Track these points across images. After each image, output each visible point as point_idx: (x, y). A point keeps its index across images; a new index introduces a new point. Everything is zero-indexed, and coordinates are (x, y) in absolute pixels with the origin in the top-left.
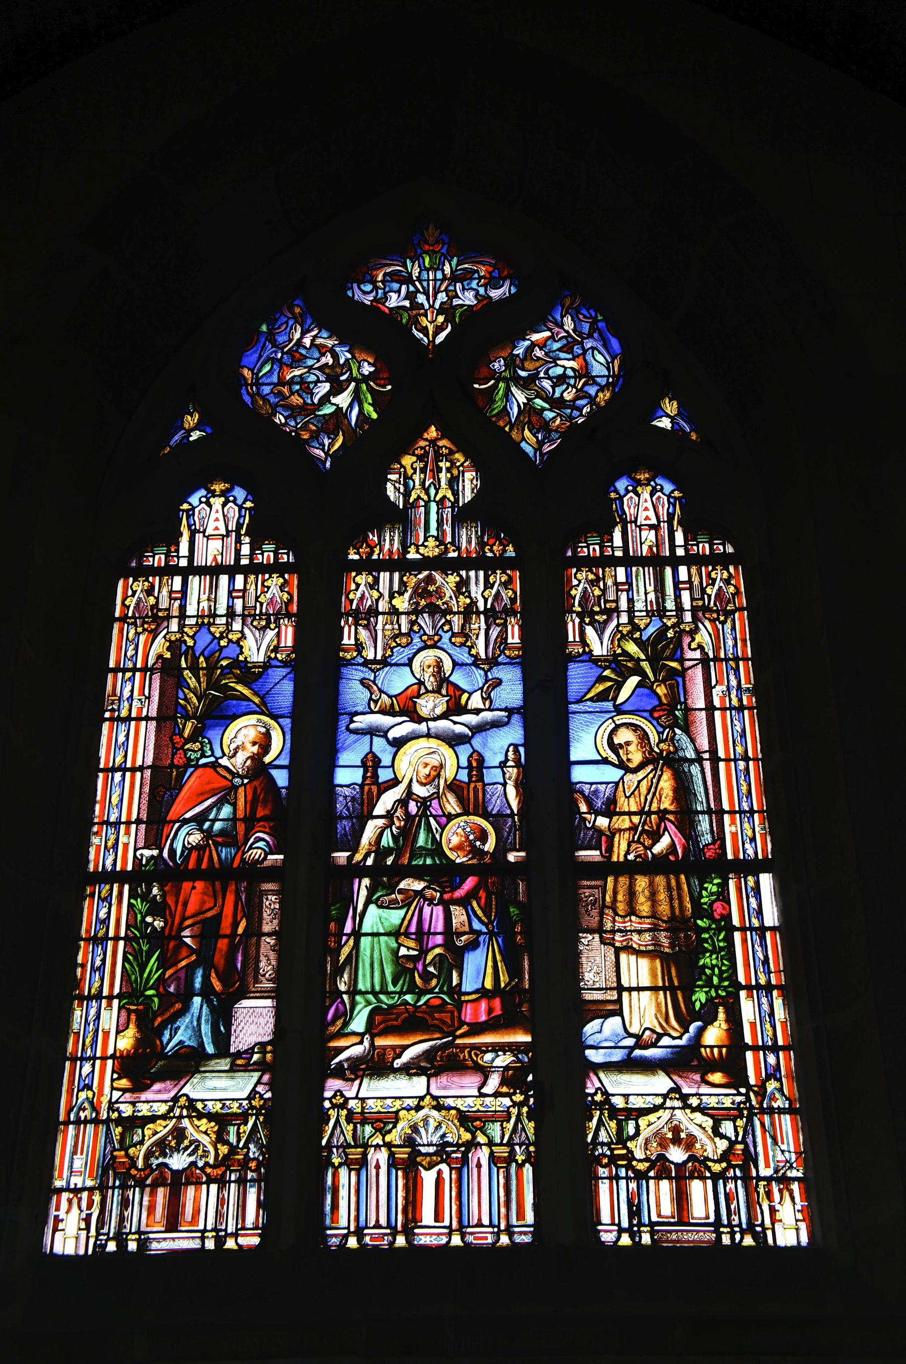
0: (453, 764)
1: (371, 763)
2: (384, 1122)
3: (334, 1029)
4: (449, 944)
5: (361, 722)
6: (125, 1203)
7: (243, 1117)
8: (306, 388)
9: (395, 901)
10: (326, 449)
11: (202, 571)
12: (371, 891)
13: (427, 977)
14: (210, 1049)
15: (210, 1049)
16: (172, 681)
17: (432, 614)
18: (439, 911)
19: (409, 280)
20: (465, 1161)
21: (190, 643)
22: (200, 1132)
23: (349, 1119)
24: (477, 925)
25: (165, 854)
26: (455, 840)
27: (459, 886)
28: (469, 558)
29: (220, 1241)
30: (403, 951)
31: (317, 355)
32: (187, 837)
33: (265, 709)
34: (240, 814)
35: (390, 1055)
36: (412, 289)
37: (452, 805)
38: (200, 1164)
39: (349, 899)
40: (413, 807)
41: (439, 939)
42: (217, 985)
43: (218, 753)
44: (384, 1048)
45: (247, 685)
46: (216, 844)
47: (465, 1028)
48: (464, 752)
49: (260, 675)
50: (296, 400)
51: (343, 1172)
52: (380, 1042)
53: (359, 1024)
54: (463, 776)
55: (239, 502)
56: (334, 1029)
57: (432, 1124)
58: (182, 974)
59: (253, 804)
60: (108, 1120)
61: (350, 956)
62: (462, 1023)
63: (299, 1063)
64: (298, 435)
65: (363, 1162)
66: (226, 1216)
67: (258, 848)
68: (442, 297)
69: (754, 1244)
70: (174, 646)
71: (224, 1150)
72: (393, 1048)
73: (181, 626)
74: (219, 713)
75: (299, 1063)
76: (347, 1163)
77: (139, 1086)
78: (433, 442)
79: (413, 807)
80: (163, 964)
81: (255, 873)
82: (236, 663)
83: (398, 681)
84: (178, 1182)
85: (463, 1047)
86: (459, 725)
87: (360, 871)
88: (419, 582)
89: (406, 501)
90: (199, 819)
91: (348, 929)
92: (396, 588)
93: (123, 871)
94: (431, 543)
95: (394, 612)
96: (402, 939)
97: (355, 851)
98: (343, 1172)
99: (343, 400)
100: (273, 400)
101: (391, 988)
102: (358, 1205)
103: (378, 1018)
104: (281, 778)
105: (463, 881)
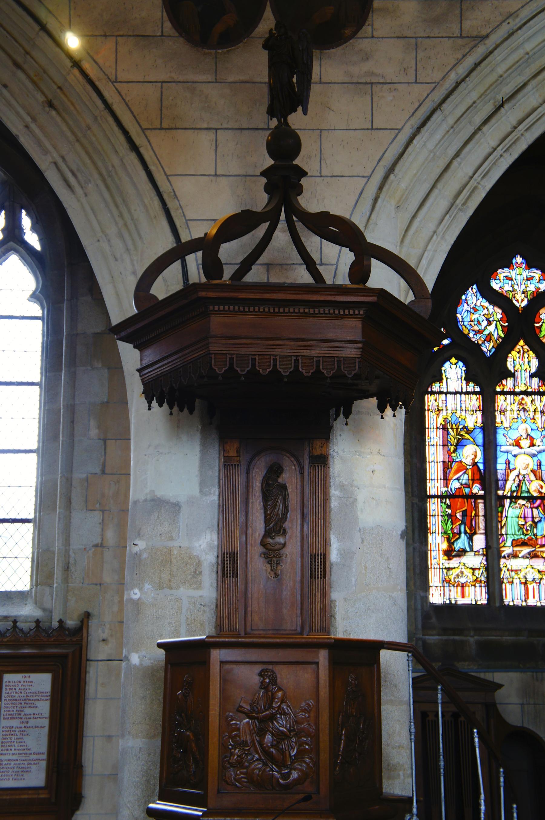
0: (532, 464)
1: (508, 463)
2: (517, 571)
3: (502, 545)
4: (533, 521)
5: (503, 449)
6: (450, 590)
7: (479, 569)
8: (479, 323)
9: (517, 507)
10: (488, 348)
11: (451, 393)
12: (510, 503)
13: (527, 530)
14: (468, 549)
15: (468, 549)
16: (446, 432)
17: (524, 411)
18: (530, 510)
19: (511, 279)
20: (540, 583)
21: (450, 419)
22: (468, 572)
23: (508, 570)
24: (541, 515)
25: (449, 490)
26: (534, 488)
27: (535, 503)
28: (535, 392)
29: (476, 602)
30: (520, 523)
31: (482, 309)
32: (455, 485)
33: (475, 443)
34: (470, 478)
35: (518, 553)
36: (513, 283)
37: (532, 477)
38: (469, 581)
39: (503, 506)
40: (521, 477)
41: (530, 519)
42: (468, 531)
43: (462, 457)
44: (516, 551)
45: (468, 434)
46: (464, 487)
47: (538, 546)
48: (535, 459)
49: (472, 431)
50: (476, 328)
51: (507, 585)
52: (515, 549)
53: (509, 543)
54: (535, 468)
55: (461, 367)
56: (502, 545)
57: (531, 573)
58: (458, 527)
59: (473, 474)
60: (442, 568)
61: (505, 524)
62: (538, 544)
63: (492, 554)
64: (478, 342)
65: (512, 582)
66: (477, 596)
67: (477, 489)
68: (523, 287)
69: (200, 254)
70: (445, 420)
71: (475, 578)
72: (519, 551)
73: (447, 413)
74: (460, 444)
75: (492, 554)
76: (509, 582)
77: (449, 559)
78: (522, 347)
79: (521, 477)
80: (452, 523)
81: (476, 497)
82: (465, 427)
83: (514, 435)
84: (463, 586)
85: (538, 551)
86: (533, 450)
87: (506, 497)
88: (519, 400)
89: (514, 370)
90: (458, 479)
91: (504, 515)
92: (512, 402)
93: (438, 495)
94: (523, 385)
95: (512, 410)
96: (520, 518)
97: (504, 490)
98: (507, 585)
99: (492, 328)
100: (469, 327)
101: (517, 533)
102: (513, 596)
103: (514, 542)
104: (481, 466)
105: (536, 501)
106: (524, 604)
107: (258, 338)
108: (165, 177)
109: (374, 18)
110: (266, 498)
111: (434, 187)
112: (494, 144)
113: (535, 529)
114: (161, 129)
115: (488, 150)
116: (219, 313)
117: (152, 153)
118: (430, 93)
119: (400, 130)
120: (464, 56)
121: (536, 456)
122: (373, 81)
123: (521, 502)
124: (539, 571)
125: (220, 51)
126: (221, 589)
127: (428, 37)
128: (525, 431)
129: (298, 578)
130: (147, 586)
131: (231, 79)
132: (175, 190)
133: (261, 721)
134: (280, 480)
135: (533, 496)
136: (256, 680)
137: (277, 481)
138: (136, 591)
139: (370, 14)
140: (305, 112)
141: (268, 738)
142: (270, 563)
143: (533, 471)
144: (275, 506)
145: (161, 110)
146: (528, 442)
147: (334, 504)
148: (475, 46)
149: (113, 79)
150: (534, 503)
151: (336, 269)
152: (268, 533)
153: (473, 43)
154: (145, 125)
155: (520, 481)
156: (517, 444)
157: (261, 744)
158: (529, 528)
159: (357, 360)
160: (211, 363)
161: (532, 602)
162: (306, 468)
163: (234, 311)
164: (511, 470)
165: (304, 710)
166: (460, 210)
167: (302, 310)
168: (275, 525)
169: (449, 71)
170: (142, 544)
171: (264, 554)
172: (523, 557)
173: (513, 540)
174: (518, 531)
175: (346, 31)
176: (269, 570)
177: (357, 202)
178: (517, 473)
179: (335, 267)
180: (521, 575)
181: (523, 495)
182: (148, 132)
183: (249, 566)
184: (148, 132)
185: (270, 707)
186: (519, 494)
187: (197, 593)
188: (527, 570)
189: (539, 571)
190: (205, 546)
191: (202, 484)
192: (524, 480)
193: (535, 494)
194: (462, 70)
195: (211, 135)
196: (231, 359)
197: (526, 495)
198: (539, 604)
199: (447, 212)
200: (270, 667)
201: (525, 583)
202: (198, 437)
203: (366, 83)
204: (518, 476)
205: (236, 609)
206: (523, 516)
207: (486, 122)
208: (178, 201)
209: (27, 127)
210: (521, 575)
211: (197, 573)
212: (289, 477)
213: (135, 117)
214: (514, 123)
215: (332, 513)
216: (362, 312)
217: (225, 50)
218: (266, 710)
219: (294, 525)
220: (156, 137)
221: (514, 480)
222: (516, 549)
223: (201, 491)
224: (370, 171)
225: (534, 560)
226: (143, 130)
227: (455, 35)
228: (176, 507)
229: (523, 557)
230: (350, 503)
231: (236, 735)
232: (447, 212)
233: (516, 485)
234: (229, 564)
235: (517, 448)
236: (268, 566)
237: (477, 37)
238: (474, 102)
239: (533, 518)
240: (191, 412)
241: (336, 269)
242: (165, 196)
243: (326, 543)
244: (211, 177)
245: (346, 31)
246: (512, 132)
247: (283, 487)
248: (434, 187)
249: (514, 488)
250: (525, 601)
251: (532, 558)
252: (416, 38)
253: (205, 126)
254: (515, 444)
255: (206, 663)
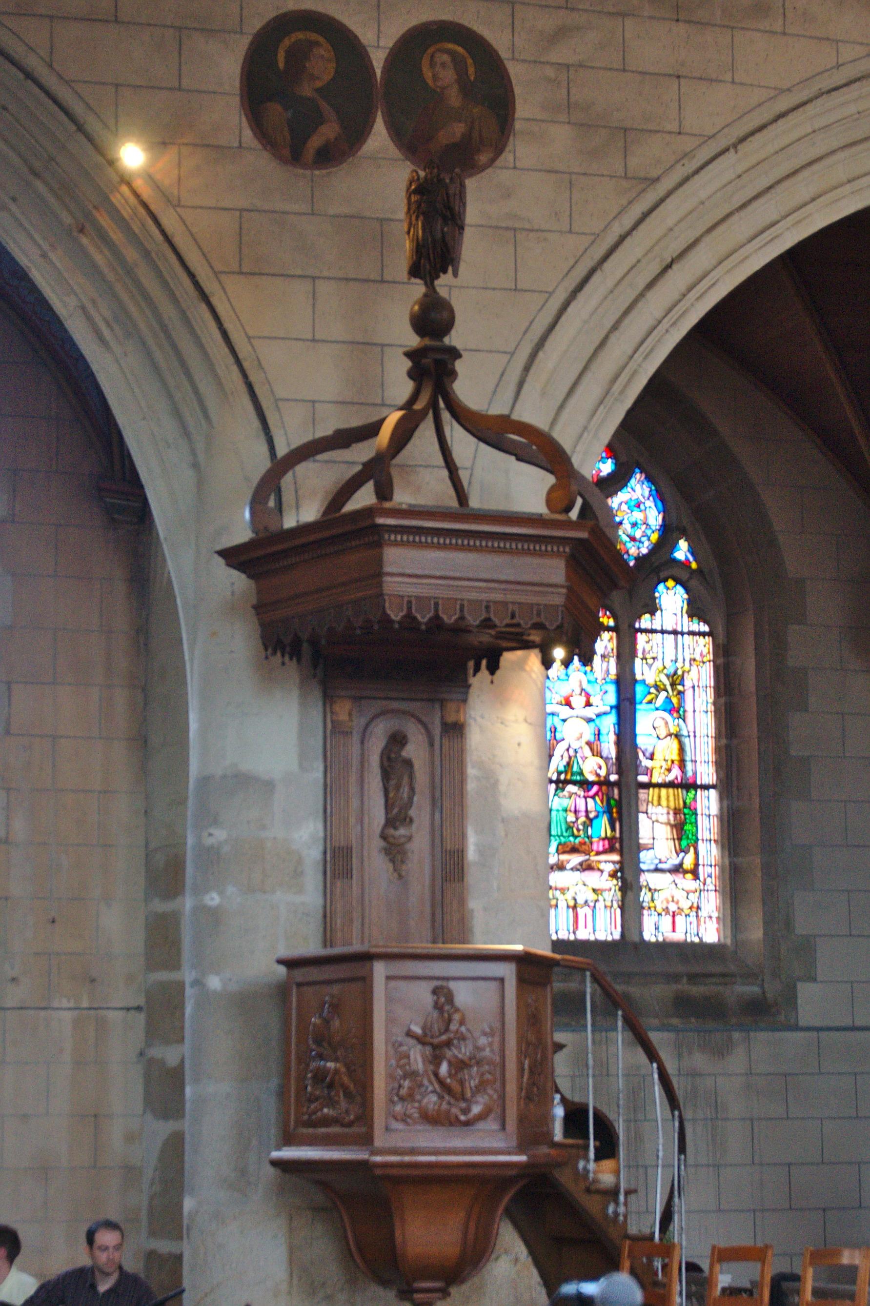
2: (563, 891)
4: (587, 816)
12: (556, 790)
13: (578, 830)
18: (583, 800)
26: (590, 769)
35: (565, 863)
37: (587, 751)
40: (571, 752)
41: (583, 814)
47: (593, 853)
54: (592, 739)
79: (571, 752)
86: (590, 712)
103: (560, 847)
106: (572, 938)
107: (460, 579)
108: (246, 340)
109: (517, 143)
110: (386, 775)
111: (586, 368)
112: (658, 314)
113: (589, 829)
114: (241, 273)
115: (651, 322)
116: (396, 544)
117: (228, 306)
118: (589, 247)
119: (551, 294)
120: (630, 203)
121: (593, 720)
122: (517, 226)
123: (571, 788)
124: (594, 890)
125: (317, 172)
126: (327, 891)
127: (585, 174)
128: (578, 684)
129: (427, 882)
130: (231, 890)
131: (332, 211)
132: (261, 359)
133: (435, 1047)
134: (404, 754)
135: (587, 780)
136: (428, 999)
137: (400, 756)
138: (215, 895)
139: (511, 138)
140: (455, 274)
141: (444, 1068)
142: (392, 861)
143: (589, 743)
144: (398, 787)
145: (240, 248)
146: (583, 699)
147: (471, 786)
148: (644, 190)
149: (175, 202)
150: (588, 791)
151: (471, 475)
152: (391, 822)
153: (643, 186)
154: (219, 267)
155: (570, 758)
156: (568, 703)
157: (436, 1074)
158: (581, 827)
159: (560, 608)
160: (384, 607)
161: (583, 934)
162: (437, 738)
163: (408, 542)
164: (558, 742)
165: (485, 1034)
166: (616, 400)
167: (502, 545)
168: (400, 812)
169: (612, 221)
170: (220, 835)
171: (385, 849)
172: (572, 869)
173: (560, 844)
174: (566, 831)
175: (481, 158)
176: (391, 869)
177: (497, 386)
178: (567, 747)
179: (469, 472)
180: (569, 895)
181: (574, 778)
182: (223, 277)
183: (366, 864)
184: (223, 277)
185: (447, 1030)
186: (569, 777)
187: (299, 899)
188: (577, 889)
189: (594, 890)
190: (306, 836)
191: (303, 756)
192: (576, 756)
193: (591, 778)
194: (628, 221)
195: (307, 286)
196: (409, 602)
197: (578, 778)
198: (592, 938)
199: (601, 403)
200: (444, 983)
201: (575, 908)
202: (295, 693)
203: (507, 228)
204: (568, 750)
205: (351, 920)
206: (573, 809)
207: (650, 285)
208: (265, 373)
209: (44, 256)
210: (569, 895)
211: (298, 874)
212: (415, 750)
213: (204, 255)
214: (683, 289)
215: (469, 797)
216: (567, 550)
217: (324, 172)
218: (441, 1034)
219: (421, 812)
220: (233, 284)
221: (562, 756)
222: (564, 857)
223: (301, 766)
224: (514, 346)
225: (587, 873)
226: (216, 274)
227: (618, 174)
228: (269, 786)
229: (572, 869)
230: (491, 782)
231: (404, 1065)
232: (601, 403)
233: (565, 763)
234: (338, 862)
235: (567, 707)
236: (391, 866)
237: (646, 179)
238: (639, 261)
239: (587, 811)
240: (299, 661)
241: (471, 475)
242: (246, 365)
243: (463, 836)
244: (309, 343)
245: (481, 158)
246: (680, 301)
247: (409, 763)
248: (586, 368)
249: (561, 768)
250: (574, 933)
251: (584, 870)
252: (570, 173)
253: (299, 272)
254: (563, 703)
255: (366, 981)
